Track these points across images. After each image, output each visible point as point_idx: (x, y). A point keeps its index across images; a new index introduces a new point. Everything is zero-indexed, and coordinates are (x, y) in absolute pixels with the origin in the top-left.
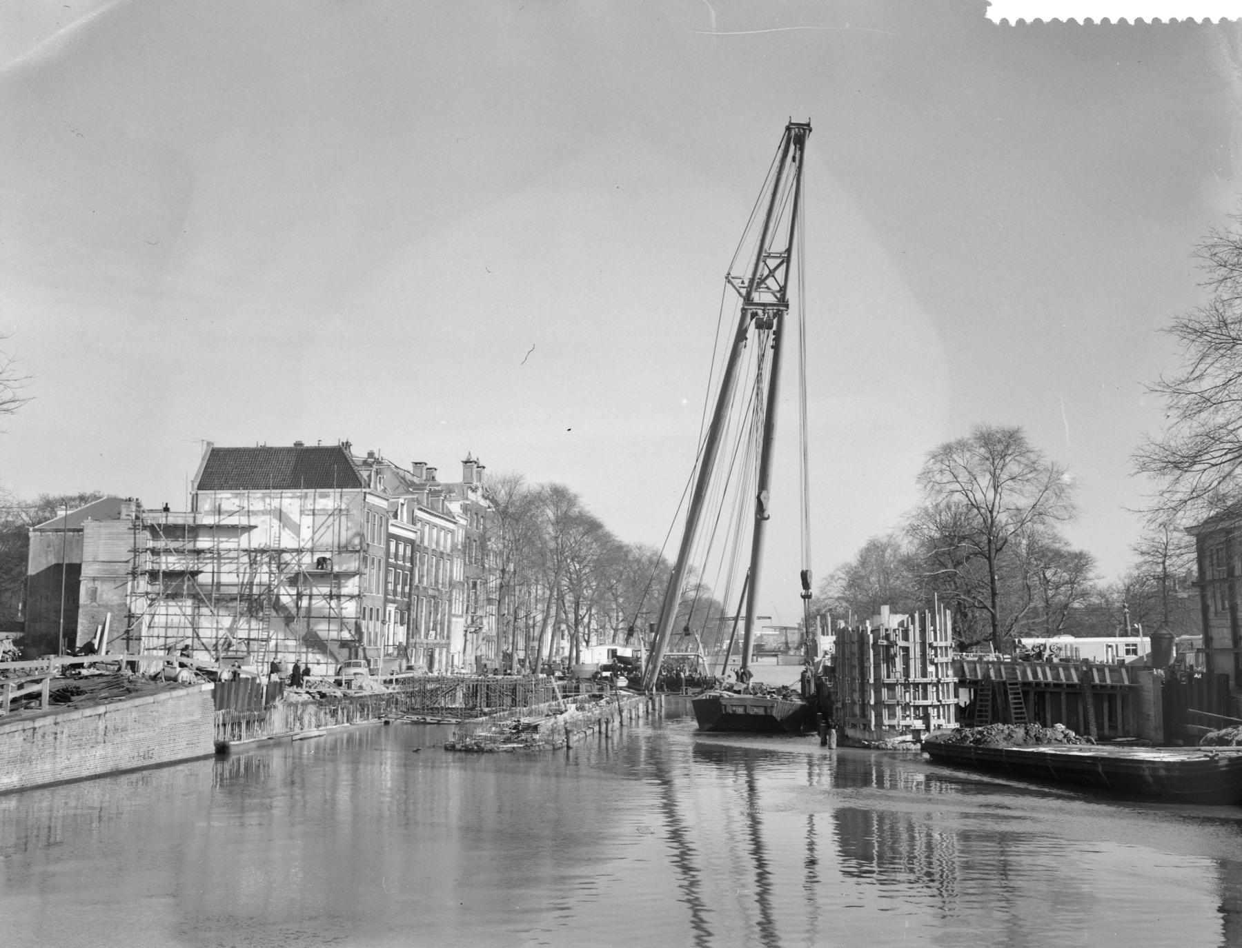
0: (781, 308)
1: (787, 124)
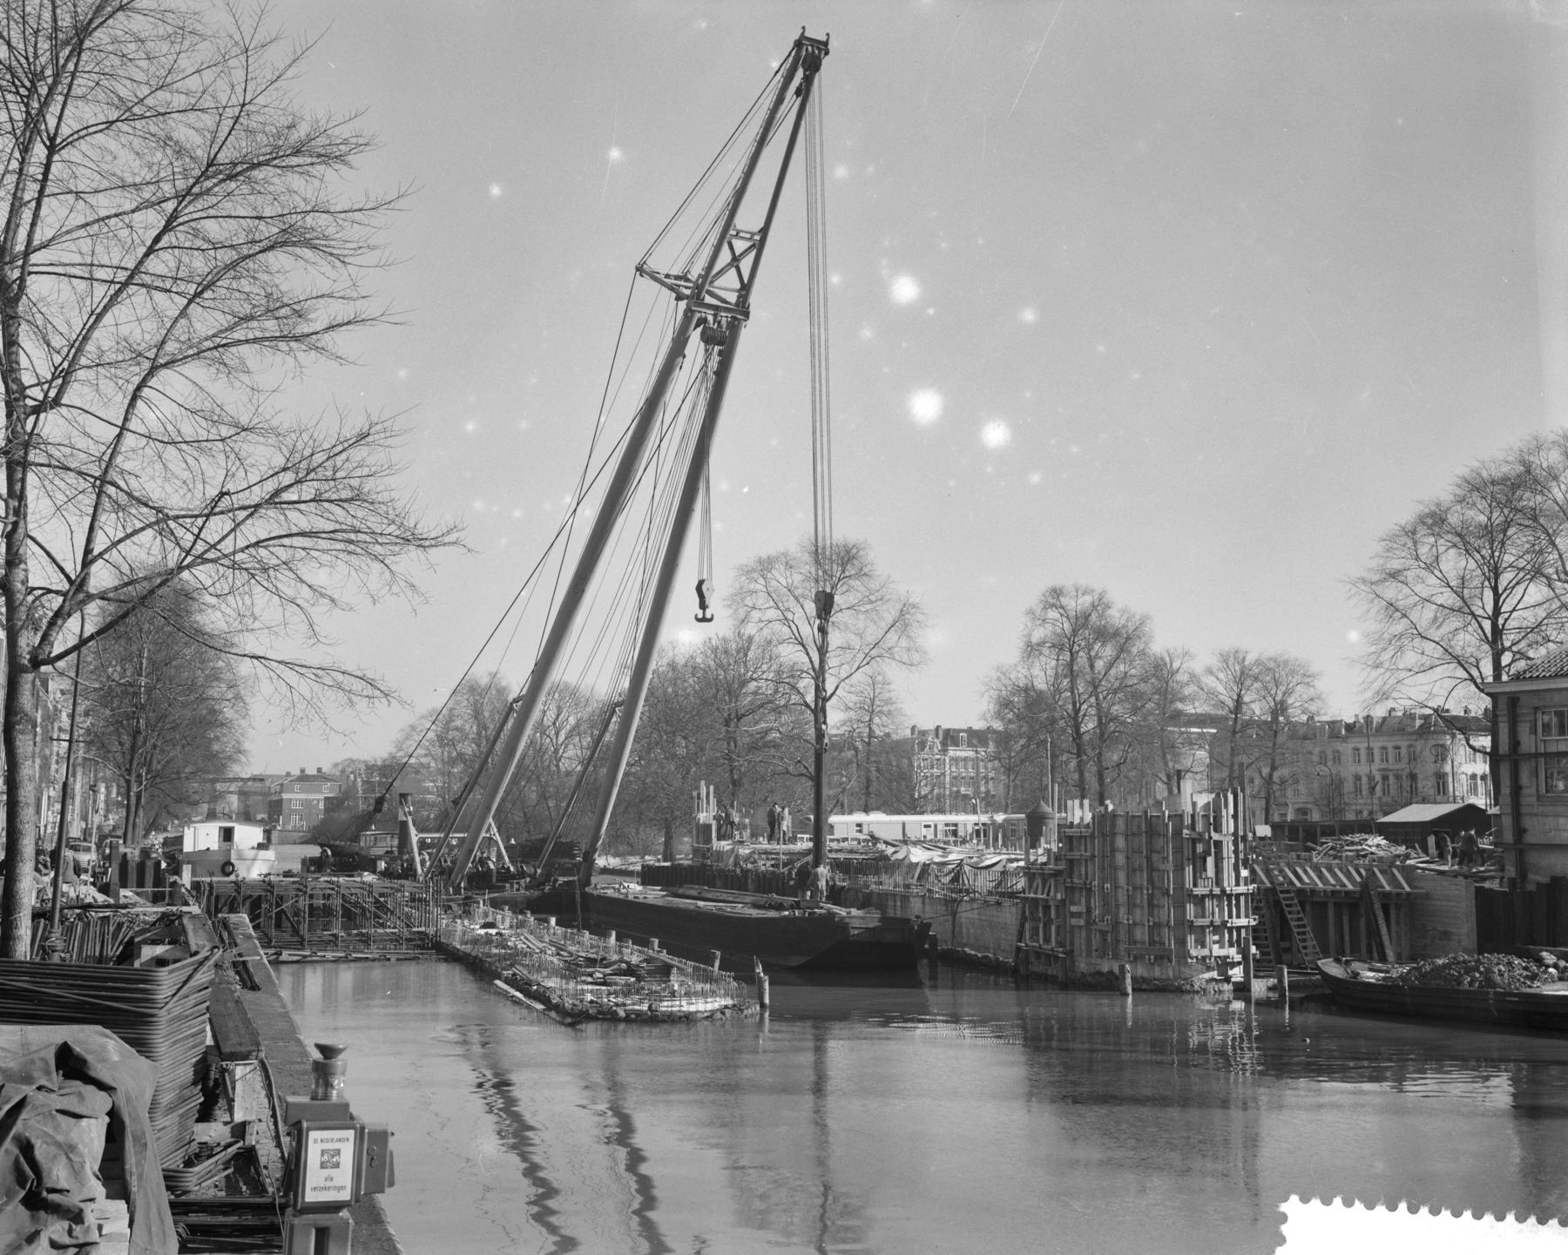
1: (797, 37)
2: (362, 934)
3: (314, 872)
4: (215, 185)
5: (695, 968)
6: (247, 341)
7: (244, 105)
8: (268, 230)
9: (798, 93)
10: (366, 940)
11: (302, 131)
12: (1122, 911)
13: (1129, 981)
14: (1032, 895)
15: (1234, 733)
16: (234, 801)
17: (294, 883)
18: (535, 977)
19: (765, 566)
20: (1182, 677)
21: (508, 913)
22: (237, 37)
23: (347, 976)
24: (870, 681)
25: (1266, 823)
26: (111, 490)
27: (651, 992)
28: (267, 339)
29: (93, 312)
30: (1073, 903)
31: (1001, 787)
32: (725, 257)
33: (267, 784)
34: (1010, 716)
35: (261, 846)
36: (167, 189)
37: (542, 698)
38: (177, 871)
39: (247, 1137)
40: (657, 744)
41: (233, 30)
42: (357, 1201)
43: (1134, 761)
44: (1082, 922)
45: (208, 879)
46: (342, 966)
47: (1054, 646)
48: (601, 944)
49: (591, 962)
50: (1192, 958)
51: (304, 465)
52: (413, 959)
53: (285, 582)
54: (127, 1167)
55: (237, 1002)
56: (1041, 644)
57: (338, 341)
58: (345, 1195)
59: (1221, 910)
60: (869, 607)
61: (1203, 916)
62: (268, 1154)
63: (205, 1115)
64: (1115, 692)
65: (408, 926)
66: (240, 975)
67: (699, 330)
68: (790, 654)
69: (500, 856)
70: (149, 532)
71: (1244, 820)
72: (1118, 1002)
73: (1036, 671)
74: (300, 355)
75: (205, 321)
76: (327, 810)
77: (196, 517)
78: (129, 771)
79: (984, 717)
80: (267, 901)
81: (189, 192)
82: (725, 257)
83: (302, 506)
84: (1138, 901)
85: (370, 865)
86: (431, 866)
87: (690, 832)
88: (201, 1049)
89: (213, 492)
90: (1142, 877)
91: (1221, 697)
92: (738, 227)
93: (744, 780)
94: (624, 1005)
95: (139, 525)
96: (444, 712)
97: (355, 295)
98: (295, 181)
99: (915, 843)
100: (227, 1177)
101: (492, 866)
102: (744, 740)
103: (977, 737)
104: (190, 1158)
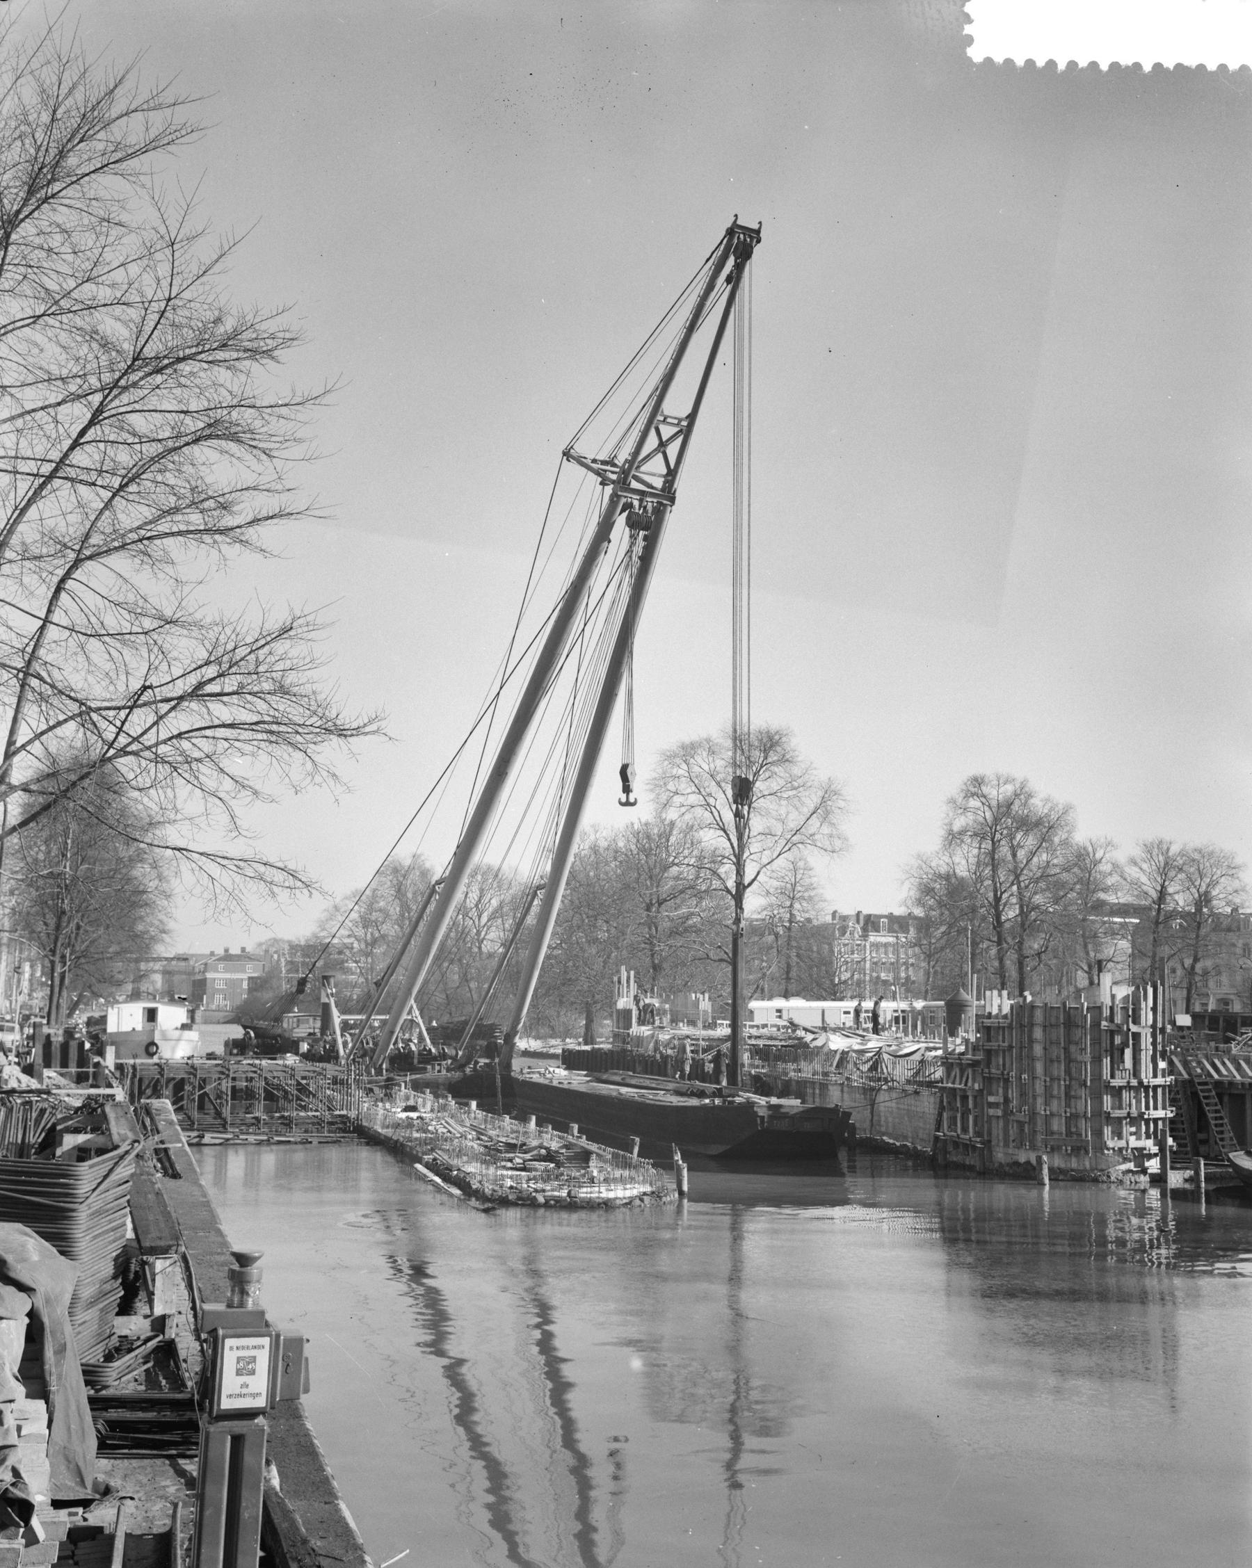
0: (665, 502)
2: (282, 1117)
3: (237, 1055)
4: (142, 379)
5: (615, 1156)
6: (172, 534)
7: (169, 299)
8: (193, 425)
9: (729, 280)
10: (288, 1123)
11: (229, 325)
12: (1040, 1101)
13: (1045, 1171)
14: (950, 1085)
15: (1157, 923)
16: (158, 979)
17: (217, 1065)
18: (455, 1162)
19: (688, 751)
20: (1105, 867)
21: (429, 1097)
22: (163, 230)
23: (269, 1159)
24: (791, 867)
25: (1187, 1012)
26: (34, 682)
27: (570, 1178)
28: (191, 532)
29: (16, 507)
30: (991, 1094)
31: (921, 973)
32: (652, 442)
33: (192, 963)
34: (931, 902)
35: (184, 1027)
36: (93, 381)
37: (465, 880)
38: (101, 1053)
39: (167, 1330)
40: (579, 927)
41: (157, 223)
42: (272, 1408)
43: (1055, 950)
44: (1000, 1113)
45: (131, 1061)
46: (264, 1148)
47: (976, 834)
48: (521, 1129)
49: (511, 1147)
50: (1108, 1149)
51: (225, 658)
52: (334, 1142)
53: (207, 773)
54: (47, 1367)
55: (158, 1194)
56: (962, 832)
57: (264, 534)
58: (261, 1402)
59: (1138, 1102)
60: (791, 793)
61: (1120, 1108)
62: (188, 1347)
63: (125, 1308)
64: (1037, 881)
65: (330, 1109)
66: (162, 1163)
67: (625, 514)
68: (712, 840)
69: (421, 1038)
70: (72, 725)
71: (1163, 1012)
72: (1034, 1193)
73: (957, 859)
74: (224, 548)
75: (130, 514)
76: (251, 990)
77: (119, 708)
78: (53, 952)
79: (904, 903)
80: (191, 1084)
81: (116, 384)
82: (652, 442)
83: (225, 699)
84: (1055, 1092)
85: (293, 1046)
86: (353, 1047)
87: (611, 1016)
88: (122, 1242)
89: (136, 685)
90: (1059, 1068)
91: (1145, 888)
92: (666, 413)
93: (664, 965)
94: (544, 1191)
95: (61, 717)
96: (368, 892)
97: (279, 487)
98: (222, 374)
99: (835, 1030)
100: (147, 1371)
101: (414, 1048)
102: (665, 925)
103: (898, 923)
104: (110, 1351)
